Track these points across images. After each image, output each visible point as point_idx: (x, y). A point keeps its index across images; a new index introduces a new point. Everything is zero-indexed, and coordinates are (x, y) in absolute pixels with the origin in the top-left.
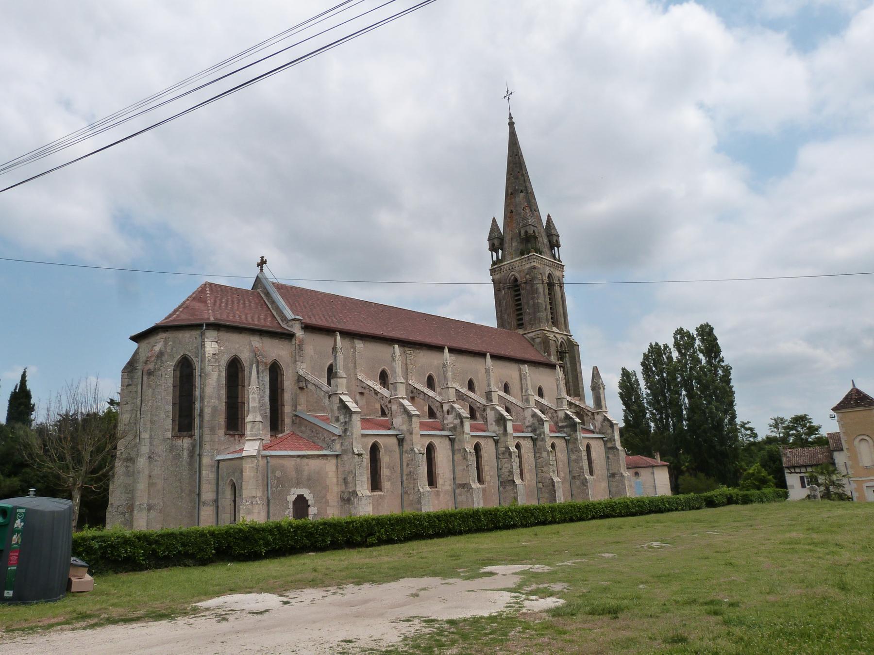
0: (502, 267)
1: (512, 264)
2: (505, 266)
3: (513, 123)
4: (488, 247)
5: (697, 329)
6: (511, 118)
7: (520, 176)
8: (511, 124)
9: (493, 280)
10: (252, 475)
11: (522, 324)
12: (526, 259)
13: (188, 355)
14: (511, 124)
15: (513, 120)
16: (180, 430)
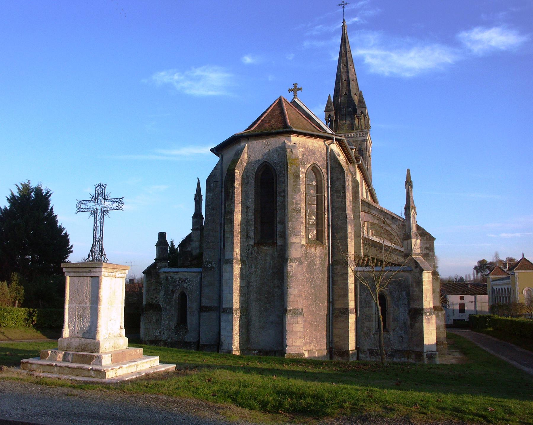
13: (318, 165)
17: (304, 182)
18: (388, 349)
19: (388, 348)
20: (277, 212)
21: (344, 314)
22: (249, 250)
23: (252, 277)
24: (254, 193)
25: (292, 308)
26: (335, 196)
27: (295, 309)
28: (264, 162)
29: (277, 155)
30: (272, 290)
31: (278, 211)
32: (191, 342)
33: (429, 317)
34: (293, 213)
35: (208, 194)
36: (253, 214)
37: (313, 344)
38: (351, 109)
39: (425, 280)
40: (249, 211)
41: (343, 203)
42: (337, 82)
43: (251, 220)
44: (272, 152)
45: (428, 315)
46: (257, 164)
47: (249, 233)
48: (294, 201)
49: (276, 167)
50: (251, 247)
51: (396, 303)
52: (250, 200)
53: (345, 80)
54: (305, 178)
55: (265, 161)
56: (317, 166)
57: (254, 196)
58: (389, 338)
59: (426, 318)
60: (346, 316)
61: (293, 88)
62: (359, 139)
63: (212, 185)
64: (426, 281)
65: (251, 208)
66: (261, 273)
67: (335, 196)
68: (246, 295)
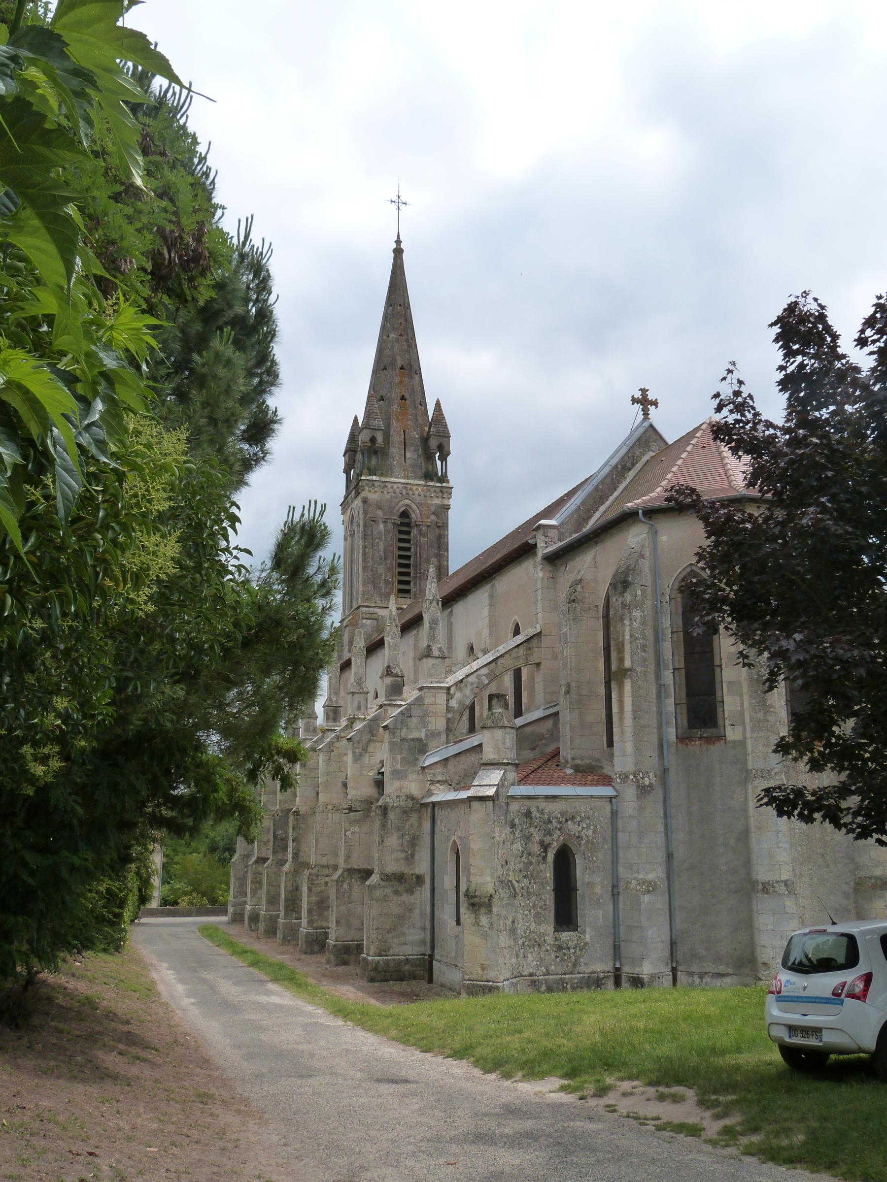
0: (389, 485)
1: (409, 486)
2: (395, 486)
3: (402, 251)
6: (398, 242)
8: (398, 252)
14: (398, 252)
15: (402, 246)
16: (692, 725)
30: (830, 838)
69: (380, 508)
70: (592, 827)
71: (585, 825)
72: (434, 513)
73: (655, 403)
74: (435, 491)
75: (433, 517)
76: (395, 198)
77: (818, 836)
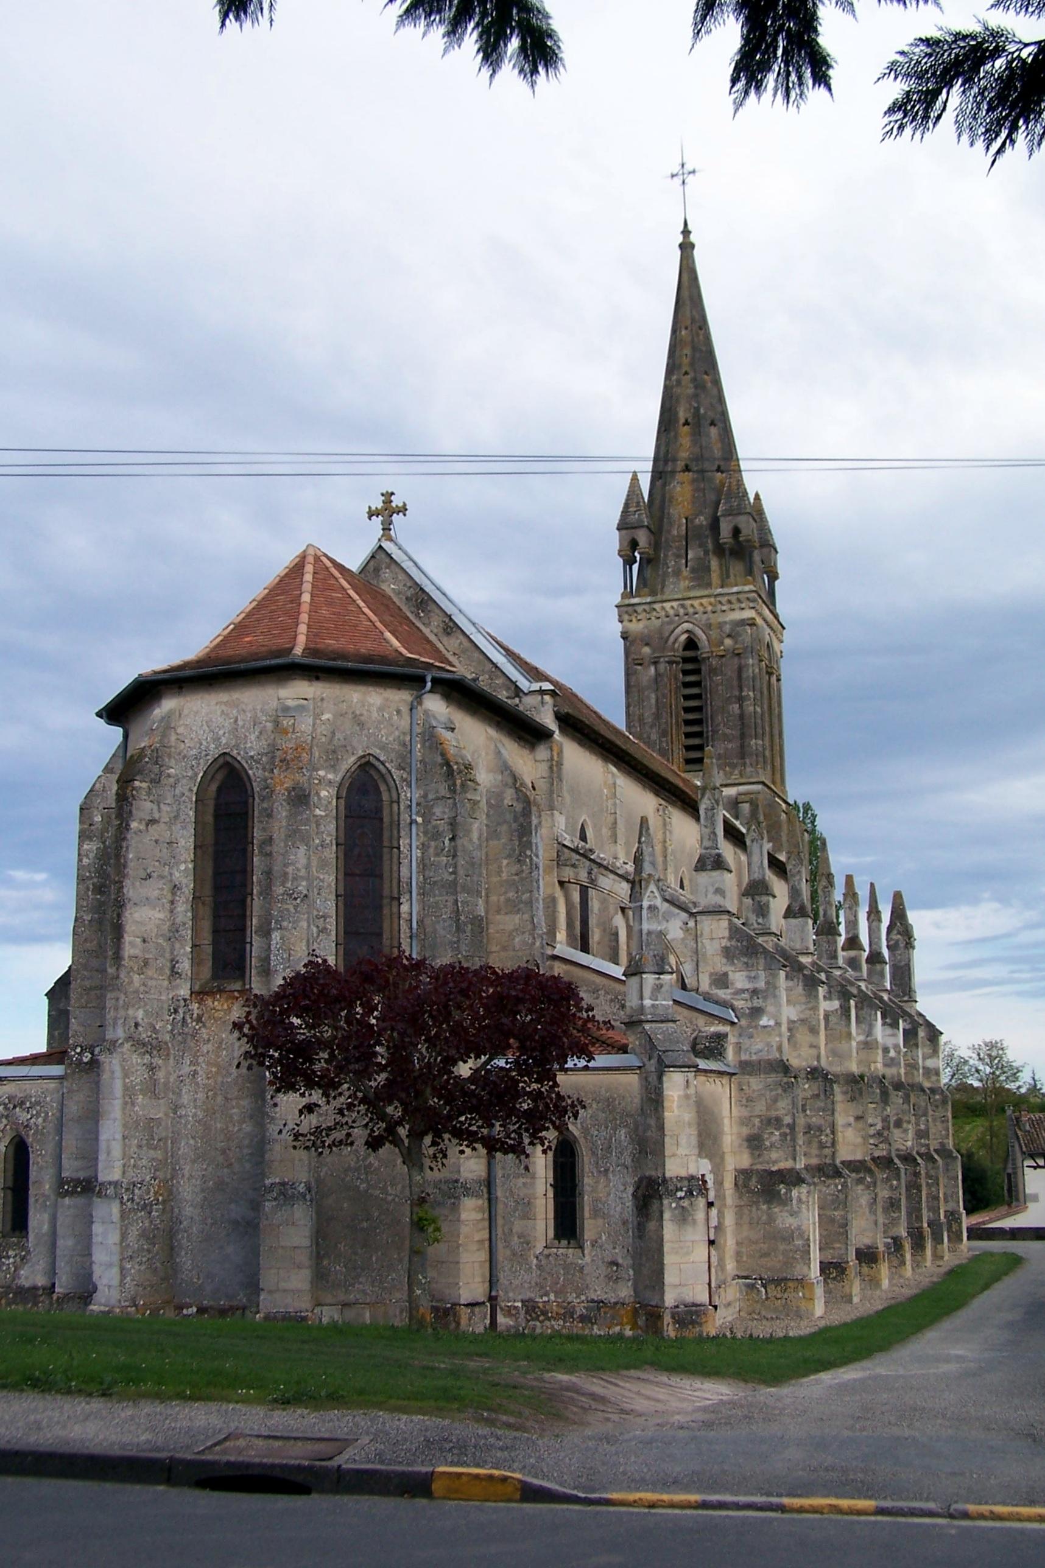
1: (688, 603)
3: (692, 246)
4: (618, 547)
5: (804, 804)
6: (686, 232)
7: (709, 385)
8: (686, 247)
9: (625, 636)
10: (687, 1119)
11: (700, 761)
12: (733, 598)
13: (378, 760)
14: (686, 247)
15: (693, 238)
17: (335, 811)
18: (578, 1301)
19: (578, 1297)
20: (252, 899)
21: (449, 1198)
22: (176, 1011)
23: (184, 1091)
24: (192, 847)
25: (277, 1180)
26: (431, 850)
27: (288, 1184)
28: (220, 756)
29: (257, 733)
30: (236, 1129)
31: (255, 897)
32: (35, 1288)
33: (685, 1203)
34: (286, 907)
35: (85, 846)
36: (189, 907)
37: (357, 1286)
38: (702, 518)
39: (671, 1093)
40: (178, 898)
41: (451, 870)
42: (663, 429)
43: (184, 924)
44: (243, 727)
45: (681, 1198)
46: (201, 761)
47: (177, 962)
48: (290, 869)
49: (251, 769)
50: (182, 1003)
51: (600, 1162)
52: (183, 867)
53: (686, 423)
54: (338, 798)
55: (225, 753)
56: (377, 763)
57: (192, 856)
58: (582, 1268)
59: (674, 1205)
60: (454, 1204)
61: (380, 505)
62: (727, 619)
63: (96, 819)
64: (676, 1099)
65: (185, 890)
66: (208, 1078)
67: (431, 850)
68: (165, 1144)
69: (647, 644)
70: (43, 1115)
71: (34, 1112)
72: (729, 636)
73: (403, 510)
74: (730, 602)
75: (728, 642)
76: (689, 167)
77: (219, 1125)
